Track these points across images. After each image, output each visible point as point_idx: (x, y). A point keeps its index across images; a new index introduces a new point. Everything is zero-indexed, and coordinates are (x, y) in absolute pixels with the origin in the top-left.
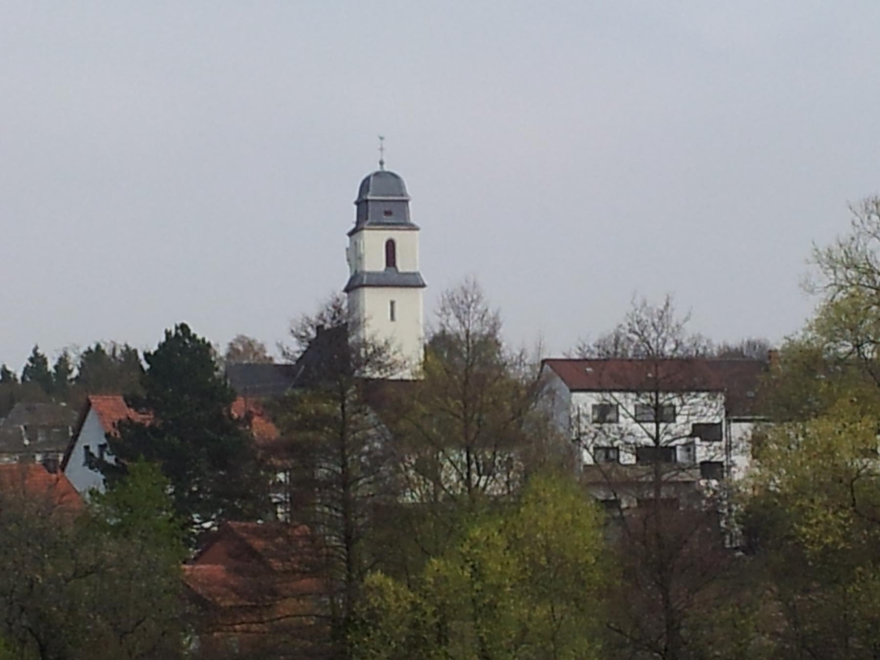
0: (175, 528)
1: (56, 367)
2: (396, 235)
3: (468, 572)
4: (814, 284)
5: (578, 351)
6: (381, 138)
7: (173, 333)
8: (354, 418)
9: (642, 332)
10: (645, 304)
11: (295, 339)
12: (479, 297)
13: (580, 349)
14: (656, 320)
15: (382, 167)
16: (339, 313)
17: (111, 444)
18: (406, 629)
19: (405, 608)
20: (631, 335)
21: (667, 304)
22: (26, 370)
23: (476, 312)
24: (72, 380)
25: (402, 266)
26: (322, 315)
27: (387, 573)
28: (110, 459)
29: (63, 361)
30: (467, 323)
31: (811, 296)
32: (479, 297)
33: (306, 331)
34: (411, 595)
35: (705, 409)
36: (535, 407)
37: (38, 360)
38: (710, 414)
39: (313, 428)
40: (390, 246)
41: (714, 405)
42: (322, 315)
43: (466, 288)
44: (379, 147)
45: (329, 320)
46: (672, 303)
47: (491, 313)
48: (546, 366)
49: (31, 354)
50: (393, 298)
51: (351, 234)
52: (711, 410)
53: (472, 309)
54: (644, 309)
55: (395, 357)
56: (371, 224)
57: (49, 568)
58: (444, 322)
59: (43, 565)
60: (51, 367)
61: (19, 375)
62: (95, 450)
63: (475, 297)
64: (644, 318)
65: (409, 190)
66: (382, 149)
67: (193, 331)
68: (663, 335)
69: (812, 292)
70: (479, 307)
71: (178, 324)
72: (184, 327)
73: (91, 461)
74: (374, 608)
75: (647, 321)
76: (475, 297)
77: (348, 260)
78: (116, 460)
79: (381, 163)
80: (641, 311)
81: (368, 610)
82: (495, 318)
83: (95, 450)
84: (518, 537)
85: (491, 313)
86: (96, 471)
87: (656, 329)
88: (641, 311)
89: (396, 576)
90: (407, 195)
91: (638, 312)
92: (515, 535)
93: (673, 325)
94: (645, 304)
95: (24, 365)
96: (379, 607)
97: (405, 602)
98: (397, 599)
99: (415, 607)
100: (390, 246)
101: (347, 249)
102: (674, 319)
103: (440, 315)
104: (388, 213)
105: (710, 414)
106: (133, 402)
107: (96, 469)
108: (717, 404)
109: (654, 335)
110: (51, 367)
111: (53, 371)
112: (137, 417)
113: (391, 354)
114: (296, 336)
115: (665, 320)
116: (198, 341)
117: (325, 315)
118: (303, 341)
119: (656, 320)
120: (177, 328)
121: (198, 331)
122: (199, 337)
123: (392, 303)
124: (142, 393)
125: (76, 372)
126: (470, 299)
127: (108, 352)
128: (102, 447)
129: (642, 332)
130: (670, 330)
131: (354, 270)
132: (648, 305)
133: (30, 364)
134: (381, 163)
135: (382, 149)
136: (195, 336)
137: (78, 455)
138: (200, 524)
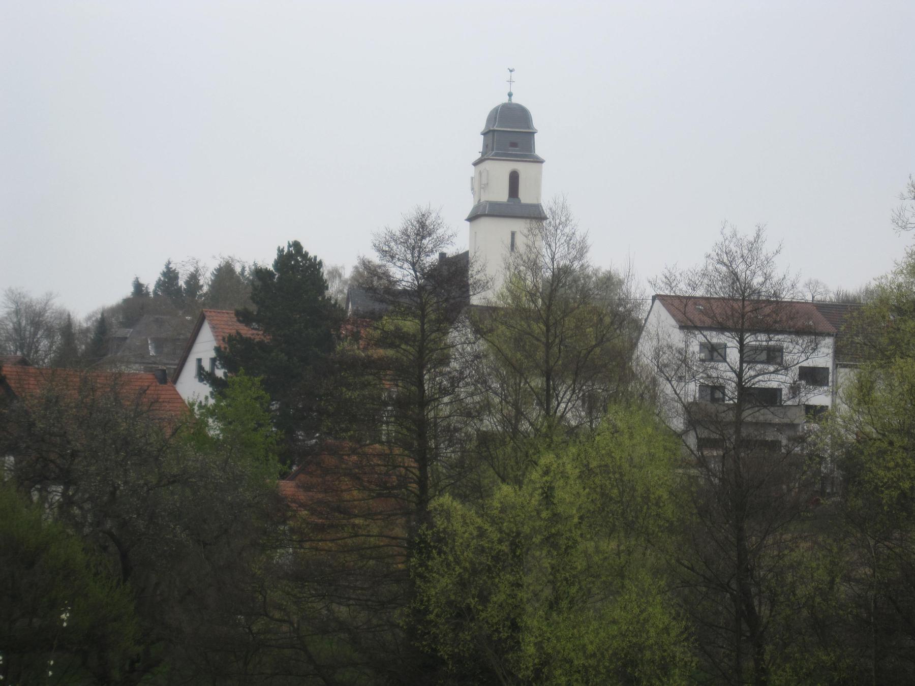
0: (271, 443)
1: (187, 283)
2: (520, 167)
3: (536, 501)
4: (908, 220)
5: (664, 279)
6: (511, 71)
7: (286, 250)
8: (433, 336)
9: (731, 262)
10: (735, 235)
11: (377, 254)
12: (567, 219)
13: (666, 277)
14: (745, 252)
15: (510, 100)
16: (423, 228)
17: (221, 356)
18: (471, 555)
19: (471, 534)
20: (718, 266)
21: (758, 236)
22: (159, 284)
23: (563, 235)
24: (201, 296)
25: (525, 197)
26: (406, 230)
27: (455, 496)
28: (220, 373)
29: (193, 279)
30: (553, 245)
31: (903, 232)
32: (567, 219)
33: (389, 247)
34: (479, 520)
35: (791, 346)
36: (731, 359)
37: (170, 276)
38: (796, 351)
39: (392, 345)
40: (514, 178)
41: (800, 342)
42: (406, 230)
43: (554, 209)
44: (509, 79)
45: (413, 237)
46: (764, 235)
47: (578, 237)
48: (657, 302)
49: (163, 268)
50: (514, 229)
51: (476, 164)
52: (797, 347)
53: (559, 231)
54: (734, 240)
55: (478, 277)
56: (496, 155)
57: (132, 474)
58: (530, 243)
59: (126, 471)
60: (182, 283)
61: (151, 288)
62: (207, 366)
63: (563, 219)
64: (734, 249)
65: (536, 123)
66: (511, 81)
67: (306, 248)
68: (752, 267)
69: (904, 228)
70: (567, 230)
71: (292, 240)
72: (297, 245)
73: (203, 375)
74: (438, 532)
75: (736, 252)
76: (563, 219)
77: (473, 189)
78: (225, 374)
79: (510, 95)
80: (730, 242)
81: (433, 533)
82: (583, 240)
83: (207, 366)
84: (591, 466)
85: (578, 237)
86: (205, 384)
87: (745, 261)
88: (730, 242)
89: (464, 498)
90: (533, 128)
91: (727, 242)
92: (587, 466)
93: (763, 258)
94: (735, 235)
95: (157, 279)
96: (444, 531)
97: (471, 528)
98: (465, 523)
99: (482, 533)
100: (514, 178)
101: (472, 178)
102: (764, 252)
103: (527, 237)
104: (514, 145)
105: (796, 351)
106: (244, 317)
107: (205, 382)
108: (804, 341)
109: (742, 267)
110: (182, 283)
111: (184, 286)
112: (246, 331)
113: (474, 273)
114: (378, 251)
115: (755, 252)
116: (310, 260)
117: (409, 229)
118: (385, 256)
119: (745, 252)
120: (289, 246)
121: (312, 249)
122: (311, 254)
123: (513, 234)
124: (253, 308)
125: (205, 289)
126: (558, 221)
127: (238, 269)
128: (213, 361)
129: (731, 262)
130: (759, 262)
131: (477, 200)
132: (738, 236)
133: (162, 279)
134: (510, 95)
135: (511, 81)
136: (307, 254)
137: (190, 369)
138: (304, 441)
